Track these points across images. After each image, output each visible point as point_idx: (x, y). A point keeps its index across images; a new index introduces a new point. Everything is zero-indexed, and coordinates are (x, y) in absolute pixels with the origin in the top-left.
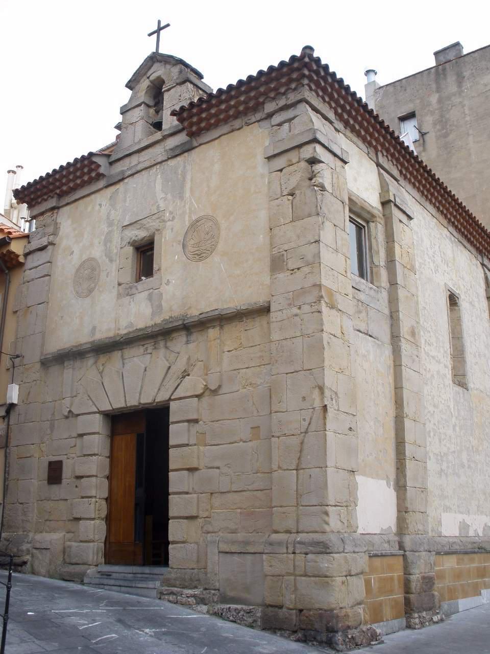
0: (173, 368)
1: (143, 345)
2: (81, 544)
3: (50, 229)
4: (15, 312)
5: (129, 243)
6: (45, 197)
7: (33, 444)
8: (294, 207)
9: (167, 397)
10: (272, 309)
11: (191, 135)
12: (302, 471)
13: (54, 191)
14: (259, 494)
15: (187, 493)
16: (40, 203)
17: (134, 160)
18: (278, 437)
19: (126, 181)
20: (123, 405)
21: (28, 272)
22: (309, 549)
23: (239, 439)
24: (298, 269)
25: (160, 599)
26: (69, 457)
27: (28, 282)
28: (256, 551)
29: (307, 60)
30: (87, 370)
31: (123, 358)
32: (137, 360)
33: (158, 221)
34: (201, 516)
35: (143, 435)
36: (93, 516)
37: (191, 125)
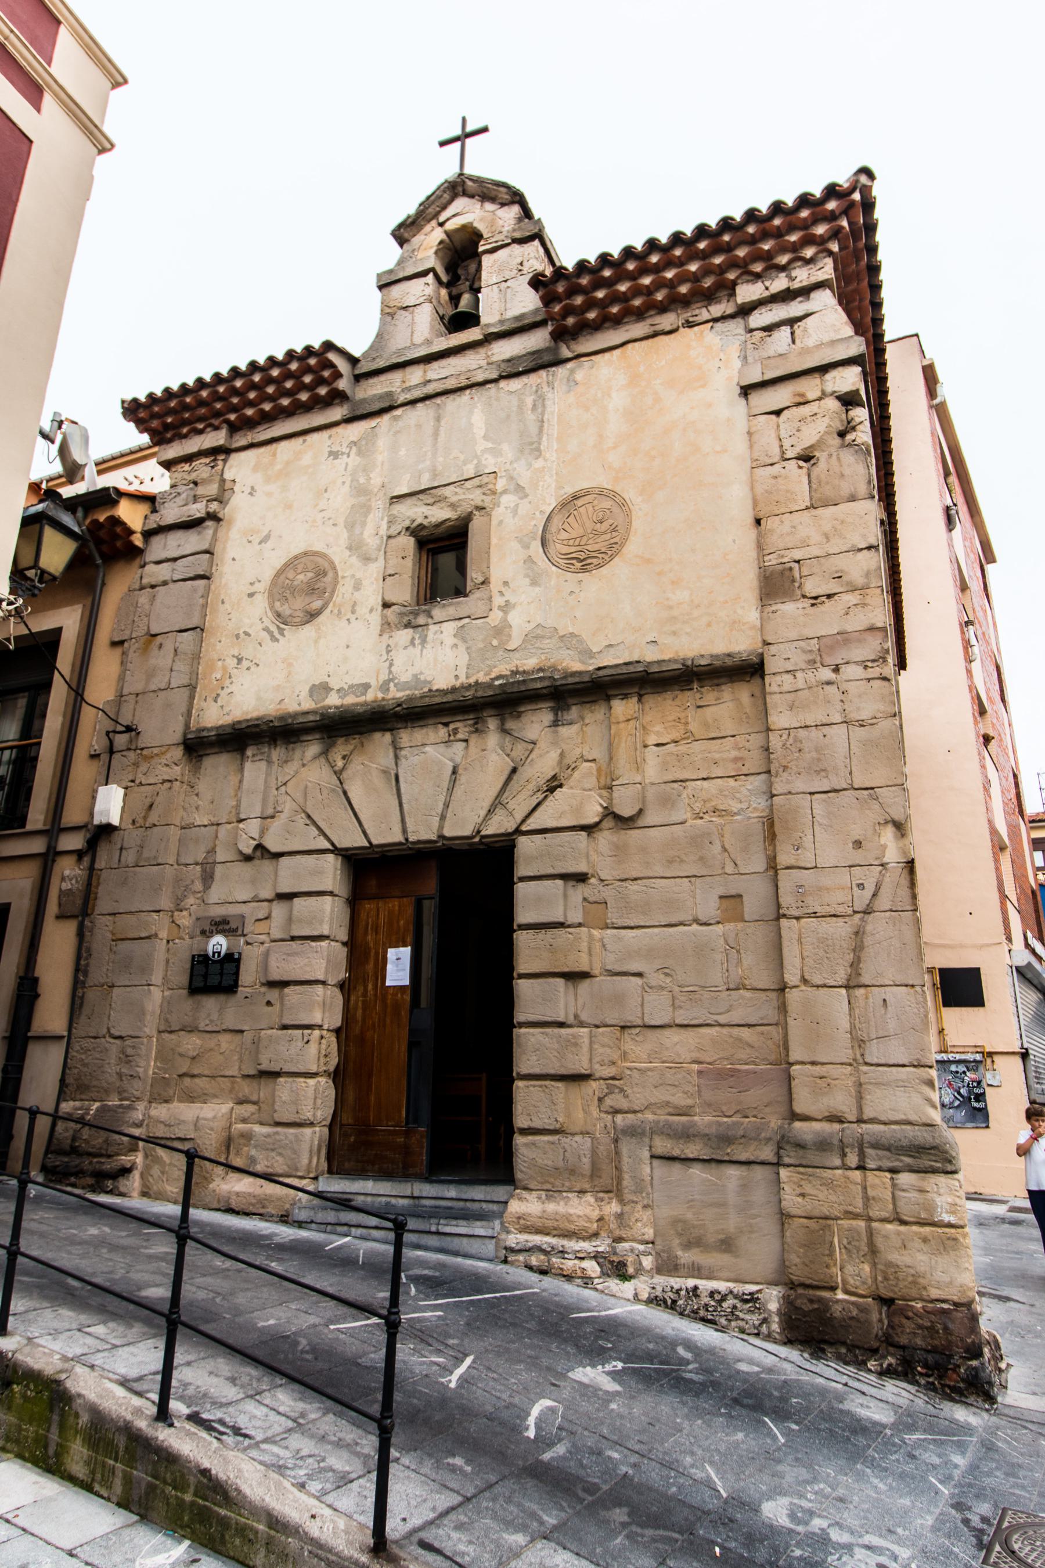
0: (525, 773)
1: (446, 725)
2: (279, 1129)
3: (213, 489)
4: (115, 644)
5: (407, 529)
6: (201, 426)
7: (158, 911)
8: (814, 480)
9: (510, 826)
10: (770, 666)
11: (561, 335)
12: (862, 991)
13: (224, 415)
14: (745, 1033)
15: (561, 1025)
16: (185, 436)
17: (415, 375)
18: (797, 918)
19: (398, 412)
20: (398, 838)
21: (150, 568)
22: (901, 1161)
23: (691, 918)
24: (829, 596)
25: (505, 1261)
26: (249, 941)
27: (153, 587)
28: (752, 1158)
29: (857, 196)
30: (304, 765)
31: (396, 748)
32: (429, 751)
33: (479, 491)
34: (597, 1075)
35: (454, 901)
36: (314, 1069)
37: (568, 311)
